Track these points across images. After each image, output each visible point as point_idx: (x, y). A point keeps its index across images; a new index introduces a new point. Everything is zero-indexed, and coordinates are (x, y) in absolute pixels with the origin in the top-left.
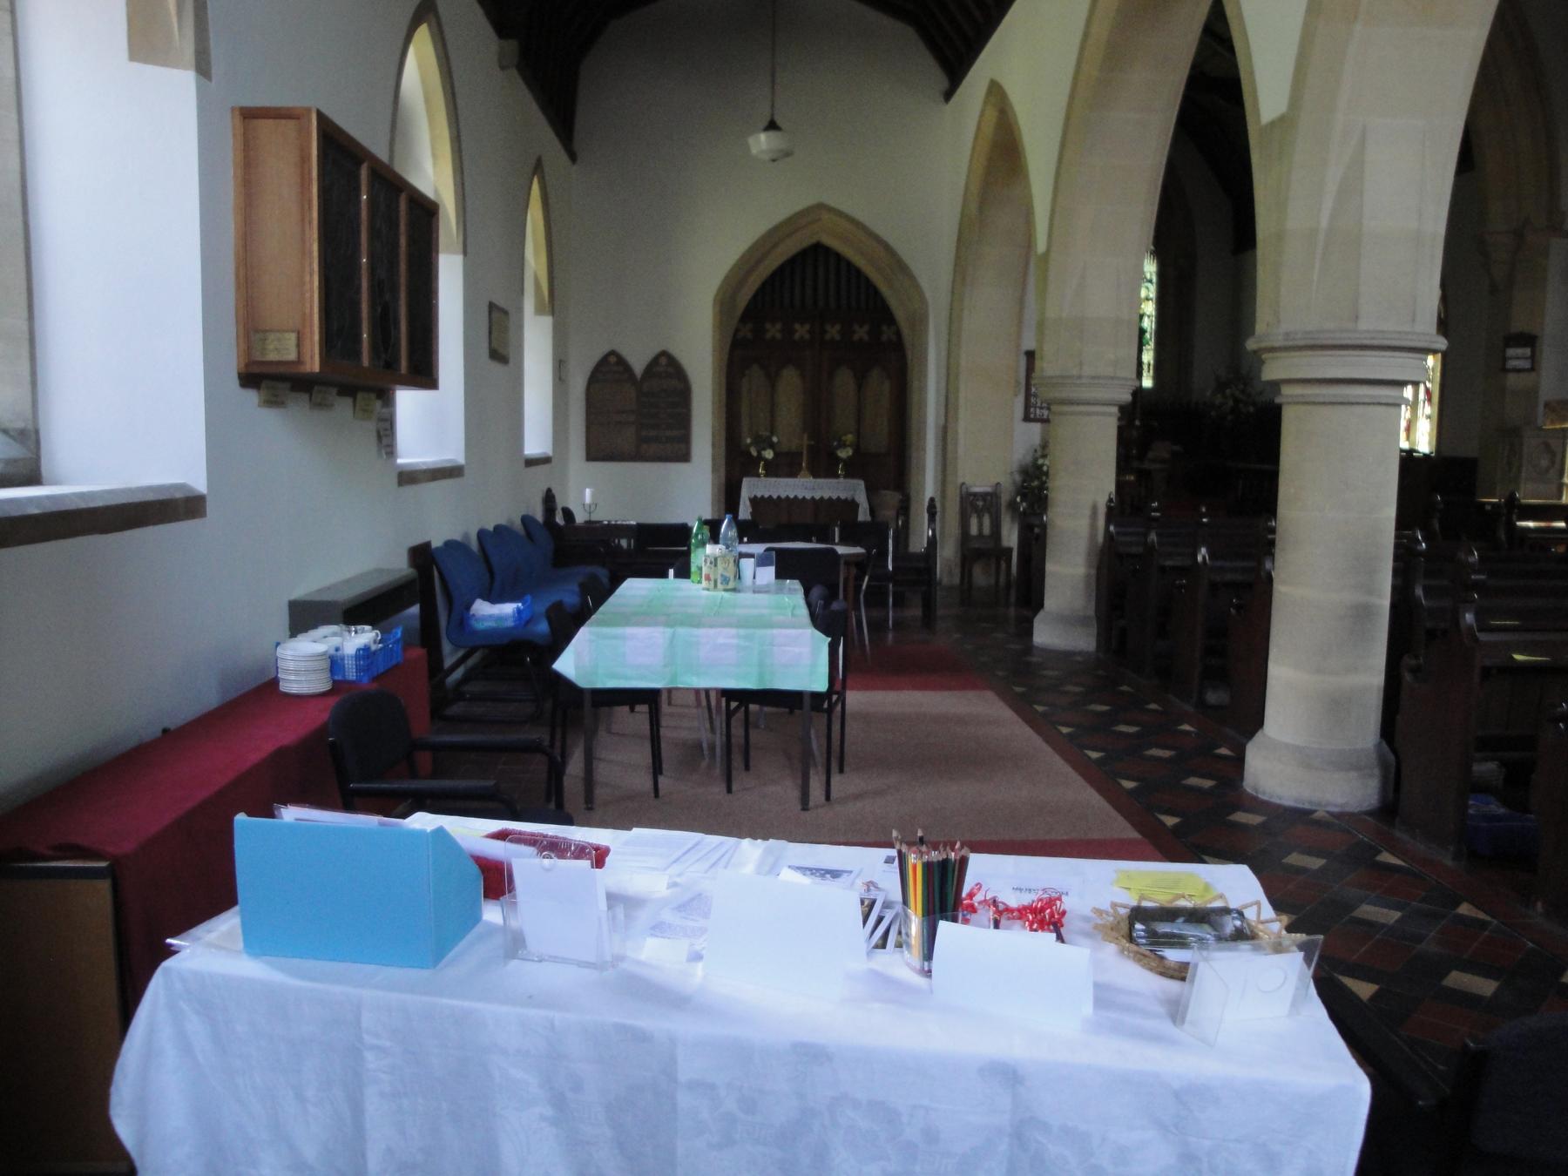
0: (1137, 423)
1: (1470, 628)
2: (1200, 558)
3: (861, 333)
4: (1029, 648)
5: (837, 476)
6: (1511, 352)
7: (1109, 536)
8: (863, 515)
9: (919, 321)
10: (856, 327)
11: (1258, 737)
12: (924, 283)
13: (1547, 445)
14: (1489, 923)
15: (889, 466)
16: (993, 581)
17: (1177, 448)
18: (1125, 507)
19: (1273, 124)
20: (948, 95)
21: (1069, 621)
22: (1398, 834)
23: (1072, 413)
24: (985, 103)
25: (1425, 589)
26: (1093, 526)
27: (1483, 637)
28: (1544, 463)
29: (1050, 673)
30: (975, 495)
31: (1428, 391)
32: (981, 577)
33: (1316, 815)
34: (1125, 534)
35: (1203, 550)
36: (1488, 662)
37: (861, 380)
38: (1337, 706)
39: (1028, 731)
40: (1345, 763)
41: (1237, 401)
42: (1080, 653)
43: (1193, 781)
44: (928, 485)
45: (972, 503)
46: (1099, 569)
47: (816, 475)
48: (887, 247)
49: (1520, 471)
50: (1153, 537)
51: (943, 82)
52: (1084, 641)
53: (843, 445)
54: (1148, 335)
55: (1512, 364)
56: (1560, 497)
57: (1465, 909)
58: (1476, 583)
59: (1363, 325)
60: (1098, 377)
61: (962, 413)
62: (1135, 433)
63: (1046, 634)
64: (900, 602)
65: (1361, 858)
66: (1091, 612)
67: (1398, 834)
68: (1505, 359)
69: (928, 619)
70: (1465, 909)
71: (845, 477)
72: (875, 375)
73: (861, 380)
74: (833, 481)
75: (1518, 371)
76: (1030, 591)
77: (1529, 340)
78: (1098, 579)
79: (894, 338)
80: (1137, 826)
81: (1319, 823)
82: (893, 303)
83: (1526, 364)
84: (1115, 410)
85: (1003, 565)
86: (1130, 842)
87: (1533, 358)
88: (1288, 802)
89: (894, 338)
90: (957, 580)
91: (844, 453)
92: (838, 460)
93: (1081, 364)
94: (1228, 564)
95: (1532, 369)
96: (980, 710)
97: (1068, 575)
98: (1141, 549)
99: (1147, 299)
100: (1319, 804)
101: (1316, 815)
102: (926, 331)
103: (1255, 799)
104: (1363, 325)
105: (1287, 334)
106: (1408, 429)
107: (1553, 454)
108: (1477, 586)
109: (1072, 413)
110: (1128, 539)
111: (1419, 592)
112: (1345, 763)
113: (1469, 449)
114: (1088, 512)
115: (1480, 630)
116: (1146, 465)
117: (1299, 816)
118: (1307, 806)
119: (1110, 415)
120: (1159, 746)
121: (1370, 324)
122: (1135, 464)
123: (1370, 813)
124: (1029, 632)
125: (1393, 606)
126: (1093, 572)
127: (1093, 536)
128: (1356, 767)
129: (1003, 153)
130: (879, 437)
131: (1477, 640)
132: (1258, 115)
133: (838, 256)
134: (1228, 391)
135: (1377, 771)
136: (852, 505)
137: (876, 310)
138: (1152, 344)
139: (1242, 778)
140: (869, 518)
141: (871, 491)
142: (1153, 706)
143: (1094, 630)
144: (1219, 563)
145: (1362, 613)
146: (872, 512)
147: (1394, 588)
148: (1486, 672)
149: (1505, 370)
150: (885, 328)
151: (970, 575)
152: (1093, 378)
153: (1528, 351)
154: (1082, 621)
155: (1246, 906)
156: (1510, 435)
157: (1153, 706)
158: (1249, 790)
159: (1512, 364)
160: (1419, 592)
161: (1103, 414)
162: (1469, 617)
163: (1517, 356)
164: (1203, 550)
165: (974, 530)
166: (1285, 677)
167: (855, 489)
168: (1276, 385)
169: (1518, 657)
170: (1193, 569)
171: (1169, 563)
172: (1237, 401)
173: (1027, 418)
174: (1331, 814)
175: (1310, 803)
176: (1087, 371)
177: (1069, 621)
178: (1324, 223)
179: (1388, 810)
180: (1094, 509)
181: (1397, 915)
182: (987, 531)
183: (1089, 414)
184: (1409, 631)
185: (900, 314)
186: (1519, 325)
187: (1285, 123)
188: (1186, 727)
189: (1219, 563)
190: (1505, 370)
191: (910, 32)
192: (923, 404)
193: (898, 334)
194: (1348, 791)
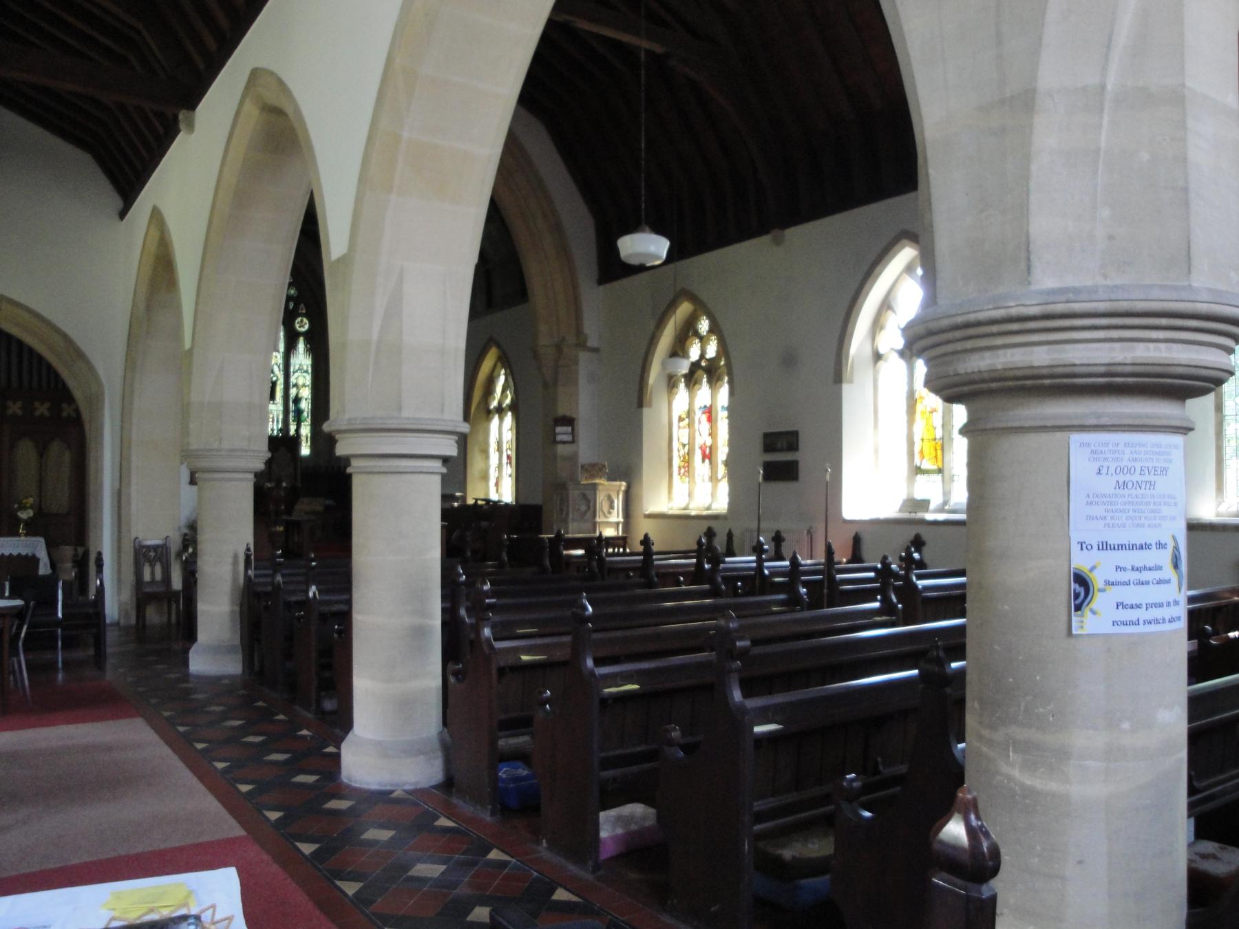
0: (284, 484)
1: (488, 640)
2: (311, 594)
3: (42, 409)
4: (186, 676)
5: (18, 535)
6: (559, 429)
7: (247, 579)
8: (44, 569)
9: (96, 400)
10: (37, 404)
11: (350, 735)
12: (101, 371)
14: (509, 862)
15: (69, 525)
16: (165, 619)
17: (328, 502)
18: (259, 557)
19: (338, 260)
20: (122, 214)
21: (217, 650)
22: (455, 801)
23: (214, 480)
24: (150, 222)
25: (467, 611)
26: (235, 572)
27: (499, 645)
28: (583, 508)
29: (200, 696)
30: (148, 547)
31: (509, 457)
32: (154, 616)
33: (394, 795)
34: (260, 576)
35: (314, 588)
36: (502, 664)
37: (42, 451)
38: (405, 706)
39: (167, 750)
40: (413, 750)
42: (230, 677)
43: (301, 778)
44: (105, 541)
45: (143, 555)
46: (241, 606)
48: (65, 337)
49: (567, 514)
50: (279, 578)
51: (119, 203)
52: (232, 666)
53: (23, 508)
54: (305, 414)
55: (559, 438)
56: (595, 531)
57: (494, 855)
58: (489, 604)
59: (405, 414)
60: (234, 450)
61: (134, 479)
62: (282, 494)
63: (200, 663)
64: (69, 644)
65: (423, 824)
66: (238, 641)
67: (455, 801)
68: (555, 435)
69: (99, 660)
70: (494, 855)
71: (26, 535)
72: (55, 447)
73: (42, 451)
74: (15, 539)
75: (564, 443)
76: (187, 629)
77: (569, 421)
78: (241, 613)
79: (73, 414)
80: (243, 823)
81: (398, 801)
82: (71, 383)
83: (568, 438)
84: (251, 476)
85: (174, 606)
86: (233, 841)
88: (374, 787)
89: (73, 414)
90: (133, 621)
91: (24, 515)
92: (19, 520)
93: (221, 440)
94: (333, 598)
95: (573, 442)
96: (132, 738)
97: (217, 612)
98: (269, 589)
99: (304, 385)
100: (397, 785)
101: (394, 795)
102: (102, 408)
103: (348, 786)
104: (405, 414)
105: (350, 419)
106: (497, 484)
107: (588, 501)
108: (491, 607)
109: (214, 480)
110: (261, 580)
111: (463, 612)
112: (413, 750)
113: (536, 500)
114: (230, 560)
115: (495, 640)
116: (295, 517)
117: (382, 796)
118: (389, 788)
119: (246, 480)
120: (278, 751)
121: (410, 412)
122: (284, 517)
123: (435, 787)
124: (186, 663)
125: (444, 624)
126: (237, 609)
127: (235, 579)
128: (421, 752)
129: (162, 268)
130: (60, 500)
131: (492, 647)
132: (329, 253)
133: (20, 343)
135: (439, 754)
136: (33, 561)
137: (59, 392)
138: (309, 420)
139: (340, 772)
140: (49, 571)
141: (50, 546)
142: (281, 717)
143: (240, 657)
144: (327, 598)
145: (419, 632)
146: (53, 565)
147: (444, 610)
148: (501, 671)
149: (555, 442)
150: (64, 406)
151: (144, 617)
152: (230, 450)
153: (569, 429)
154: (230, 650)
155: (204, 911)
156: (559, 488)
157: (281, 717)
158: (345, 780)
159: (559, 438)
160: (463, 612)
162: (487, 632)
163: (563, 432)
164: (314, 588)
165: (147, 577)
166: (369, 688)
167: (37, 547)
168: (346, 461)
169: (524, 658)
170: (306, 604)
171: (294, 598)
174: (406, 792)
175: (380, 784)
176: (226, 445)
177: (217, 650)
178: (375, 337)
179: (448, 784)
180: (236, 557)
181: (443, 868)
182: (158, 576)
183: (231, 480)
184: (457, 645)
185: (78, 394)
186: (562, 410)
187: (344, 260)
188: (305, 732)
189: (327, 598)
190: (555, 442)
191: (82, 160)
192: (99, 471)
193: (77, 411)
194: (418, 772)
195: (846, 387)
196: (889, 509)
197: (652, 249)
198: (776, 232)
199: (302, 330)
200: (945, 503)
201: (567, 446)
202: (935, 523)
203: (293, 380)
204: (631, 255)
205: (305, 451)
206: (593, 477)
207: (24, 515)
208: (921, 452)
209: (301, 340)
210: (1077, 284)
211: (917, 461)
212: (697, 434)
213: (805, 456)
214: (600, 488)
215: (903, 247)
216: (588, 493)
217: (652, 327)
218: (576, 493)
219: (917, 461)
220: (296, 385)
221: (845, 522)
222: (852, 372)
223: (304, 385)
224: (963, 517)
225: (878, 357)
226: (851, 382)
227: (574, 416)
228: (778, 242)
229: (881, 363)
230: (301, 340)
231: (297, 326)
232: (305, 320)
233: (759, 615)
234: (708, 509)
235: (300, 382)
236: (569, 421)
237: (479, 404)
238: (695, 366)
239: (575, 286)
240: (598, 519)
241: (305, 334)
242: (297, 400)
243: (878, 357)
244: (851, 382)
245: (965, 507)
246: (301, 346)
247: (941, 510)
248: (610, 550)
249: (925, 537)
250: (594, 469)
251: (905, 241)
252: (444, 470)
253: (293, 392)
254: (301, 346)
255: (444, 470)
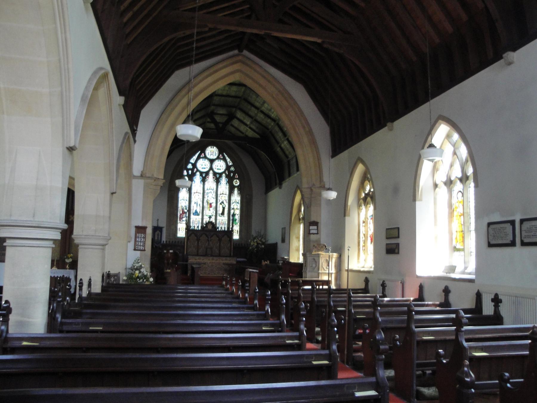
5: (66, 269)
6: (311, 227)
13: (314, 259)
28: (314, 265)
41: (258, 244)
47: (58, 268)
54: (237, 221)
55: (312, 232)
56: (318, 277)
68: (310, 230)
75: (314, 234)
77: (316, 224)
83: (315, 232)
87: (317, 229)
95: (317, 234)
99: (237, 209)
107: (316, 262)
134: (255, 240)
149: (309, 234)
152: (86, 235)
153: (316, 227)
159: (312, 232)
161: (96, 249)
172: (258, 244)
173: (135, 250)
176: (85, 233)
186: (313, 219)
190: (309, 234)
195: (418, 203)
196: (439, 272)
197: (190, 132)
198: (389, 124)
199: (236, 185)
200: (466, 268)
201: (315, 235)
202: (455, 280)
203: (232, 206)
204: (181, 135)
205: (236, 236)
206: (319, 250)
207: (68, 261)
208: (456, 238)
209: (236, 189)
210: (314, 131)
211: (454, 243)
212: (369, 229)
213: (402, 241)
214: (321, 256)
215: (440, 125)
216: (316, 258)
217: (348, 177)
218: (311, 258)
219: (454, 243)
220: (233, 209)
221: (418, 277)
222: (421, 195)
223: (237, 209)
224: (473, 277)
225: (436, 186)
226: (421, 200)
227: (318, 221)
228: (391, 130)
229: (437, 189)
230: (236, 189)
231: (234, 183)
232: (238, 181)
233: (159, 333)
234: (363, 267)
235: (235, 207)
236: (316, 224)
237: (296, 216)
238: (367, 195)
239: (319, 159)
240: (320, 271)
241: (238, 187)
242: (234, 215)
243: (436, 186)
244: (421, 200)
245: (474, 271)
246: (236, 191)
247: (463, 273)
248: (321, 287)
249: (450, 288)
250: (324, 248)
251: (440, 121)
252: (54, 246)
253: (232, 212)
254: (236, 191)
255: (54, 246)
